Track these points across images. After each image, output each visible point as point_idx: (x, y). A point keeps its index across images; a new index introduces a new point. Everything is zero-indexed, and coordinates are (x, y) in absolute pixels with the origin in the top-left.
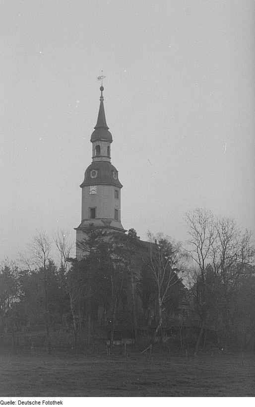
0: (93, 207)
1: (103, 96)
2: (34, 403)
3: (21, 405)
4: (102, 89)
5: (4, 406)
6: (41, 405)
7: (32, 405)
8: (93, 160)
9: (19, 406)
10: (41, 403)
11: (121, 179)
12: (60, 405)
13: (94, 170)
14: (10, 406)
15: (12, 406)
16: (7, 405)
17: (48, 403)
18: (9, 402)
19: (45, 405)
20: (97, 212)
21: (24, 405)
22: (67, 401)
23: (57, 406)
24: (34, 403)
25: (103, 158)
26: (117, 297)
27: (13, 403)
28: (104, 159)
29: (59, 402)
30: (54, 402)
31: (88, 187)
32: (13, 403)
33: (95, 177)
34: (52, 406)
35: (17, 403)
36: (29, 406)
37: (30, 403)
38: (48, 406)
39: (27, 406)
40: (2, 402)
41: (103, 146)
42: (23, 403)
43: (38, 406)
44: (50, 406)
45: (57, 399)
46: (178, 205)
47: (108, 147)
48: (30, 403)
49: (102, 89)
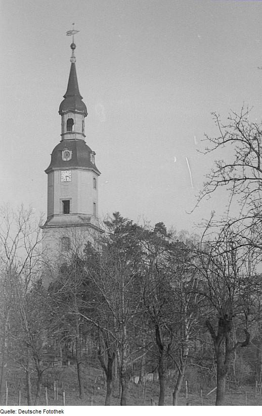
0: (66, 198)
1: (75, 56)
2: (34, 412)
3: (22, 414)
4: (73, 47)
5: (4, 415)
6: (42, 414)
7: (32, 414)
8: (63, 138)
9: (20, 415)
10: (42, 412)
11: (98, 161)
12: (61, 414)
13: (67, 151)
14: (10, 414)
15: (12, 414)
16: (7, 414)
17: (49, 412)
18: (9, 411)
19: (45, 414)
20: (72, 205)
21: (25, 414)
22: (68, 410)
23: (58, 414)
24: (34, 412)
25: (77, 135)
26: (127, 302)
27: (13, 412)
28: (79, 137)
29: (60, 411)
30: (55, 411)
31: (60, 172)
32: (13, 412)
33: (68, 159)
34: (53, 415)
35: (17, 412)
36: (30, 415)
37: (31, 412)
38: (49, 414)
39: (28, 415)
40: (2, 411)
41: (77, 118)
42: (23, 412)
43: (39, 414)
44: (51, 415)
45: (59, 408)
46: (162, 179)
47: (83, 121)
48: (31, 412)
49: (73, 47)
